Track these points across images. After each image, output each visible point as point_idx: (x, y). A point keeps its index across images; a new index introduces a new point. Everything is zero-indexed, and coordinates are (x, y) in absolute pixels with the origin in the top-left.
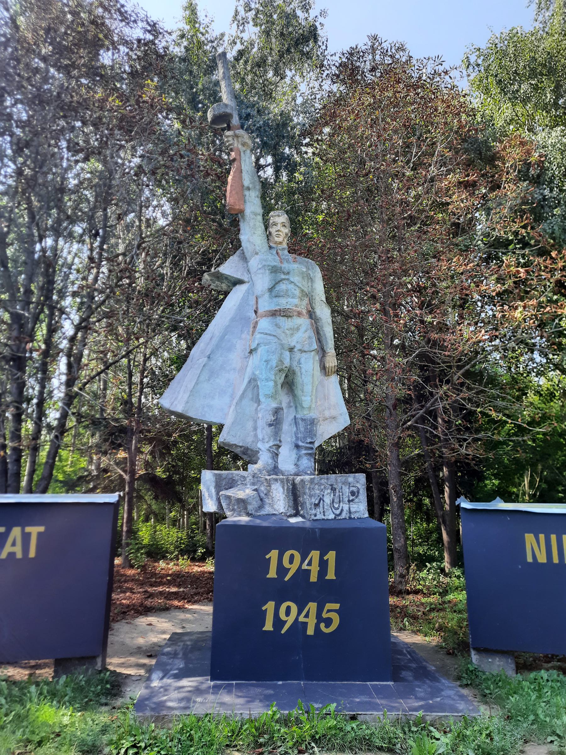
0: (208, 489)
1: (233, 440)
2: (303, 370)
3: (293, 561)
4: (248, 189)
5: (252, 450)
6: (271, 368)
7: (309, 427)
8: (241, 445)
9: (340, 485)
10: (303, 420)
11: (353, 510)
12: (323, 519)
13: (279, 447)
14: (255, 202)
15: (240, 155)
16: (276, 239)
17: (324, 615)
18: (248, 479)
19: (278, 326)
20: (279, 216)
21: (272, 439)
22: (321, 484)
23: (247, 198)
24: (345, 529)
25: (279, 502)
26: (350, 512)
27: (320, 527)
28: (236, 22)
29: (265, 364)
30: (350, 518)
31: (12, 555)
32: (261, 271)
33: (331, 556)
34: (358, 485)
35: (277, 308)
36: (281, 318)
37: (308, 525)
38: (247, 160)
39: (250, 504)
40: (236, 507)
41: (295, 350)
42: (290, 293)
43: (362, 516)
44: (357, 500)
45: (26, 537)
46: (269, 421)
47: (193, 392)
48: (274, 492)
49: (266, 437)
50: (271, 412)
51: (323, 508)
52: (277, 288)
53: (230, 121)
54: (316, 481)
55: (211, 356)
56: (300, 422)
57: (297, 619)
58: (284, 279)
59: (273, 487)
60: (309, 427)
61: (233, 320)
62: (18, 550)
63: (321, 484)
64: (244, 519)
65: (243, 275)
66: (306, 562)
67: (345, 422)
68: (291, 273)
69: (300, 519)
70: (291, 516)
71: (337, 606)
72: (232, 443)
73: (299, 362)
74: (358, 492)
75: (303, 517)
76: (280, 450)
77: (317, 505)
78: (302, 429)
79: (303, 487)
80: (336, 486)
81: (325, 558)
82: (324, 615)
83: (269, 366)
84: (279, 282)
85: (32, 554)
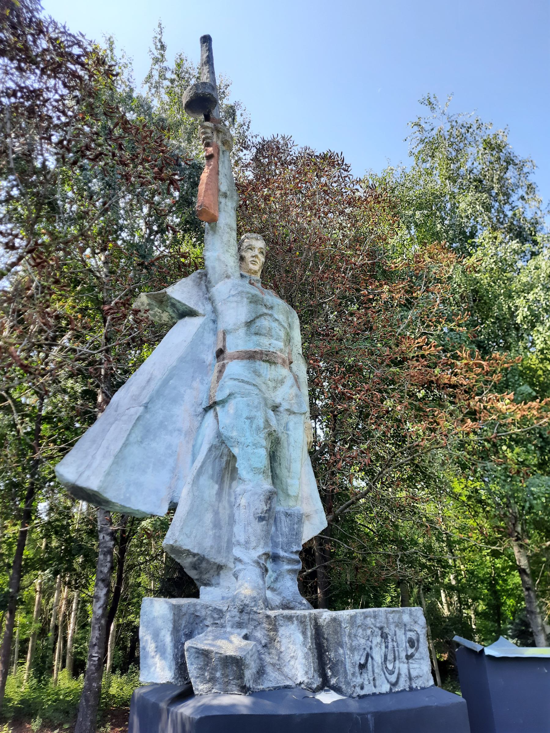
0: (156, 636)
1: (187, 544)
2: (291, 440)
4: (225, 195)
5: (208, 562)
6: (258, 429)
7: (296, 526)
8: (196, 551)
9: (392, 627)
10: (287, 515)
11: (414, 673)
12: (374, 694)
14: (231, 214)
15: (218, 154)
16: (251, 266)
18: (228, 616)
19: (257, 373)
20: (257, 239)
23: (222, 206)
24: (409, 711)
26: (410, 679)
27: (372, 709)
28: (148, 84)
29: (248, 422)
30: (411, 688)
32: (235, 299)
35: (258, 349)
36: (262, 363)
37: (354, 707)
38: (226, 162)
40: (218, 674)
41: (281, 409)
42: (273, 333)
46: (260, 511)
47: (119, 458)
48: (284, 641)
49: (253, 539)
50: (262, 497)
52: (258, 323)
53: (210, 112)
54: (359, 621)
55: (149, 406)
56: (283, 518)
58: (266, 314)
59: (282, 631)
61: (182, 360)
64: (238, 701)
65: (196, 304)
67: (322, 523)
68: (276, 308)
73: (286, 428)
75: (337, 689)
77: (363, 667)
78: (286, 530)
79: (336, 632)
83: (254, 426)
84: (261, 316)
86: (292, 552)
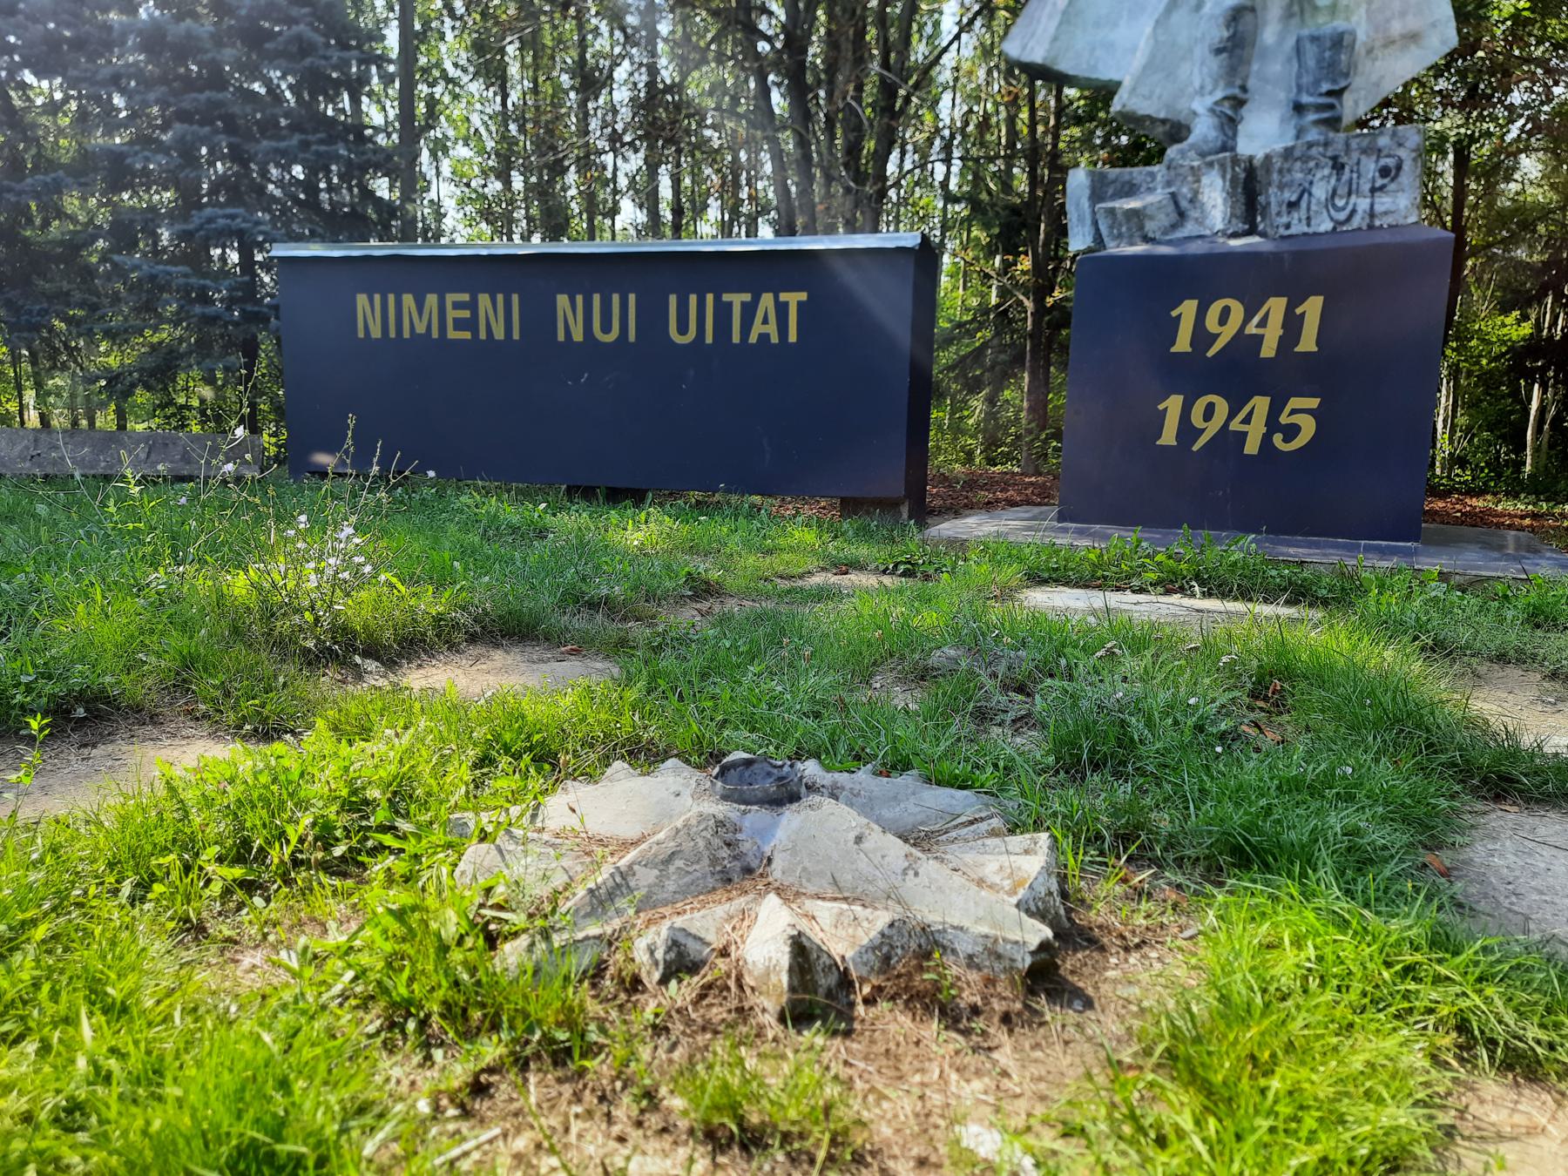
1: (1143, 107)
3: (1226, 321)
8: (1162, 115)
11: (1378, 208)
12: (1305, 234)
13: (1238, 103)
17: (1284, 419)
21: (1222, 84)
22: (1310, 158)
25: (1215, 201)
30: (1371, 227)
31: (764, 337)
33: (1313, 308)
34: (1402, 153)
39: (1151, 218)
43: (1401, 222)
44: (1392, 186)
45: (782, 309)
50: (1221, 20)
51: (1308, 209)
57: (1226, 425)
59: (1205, 180)
60: (1327, 54)
62: (772, 329)
63: (1310, 158)
66: (1256, 319)
67: (1444, 42)
69: (1255, 239)
70: (1235, 235)
71: (1313, 403)
72: (1141, 112)
74: (1399, 168)
75: (1263, 235)
76: (1244, 111)
77: (1293, 205)
78: (1311, 63)
80: (1344, 159)
81: (1298, 311)
82: (1284, 419)
85: (793, 338)
86: (1321, 95)
